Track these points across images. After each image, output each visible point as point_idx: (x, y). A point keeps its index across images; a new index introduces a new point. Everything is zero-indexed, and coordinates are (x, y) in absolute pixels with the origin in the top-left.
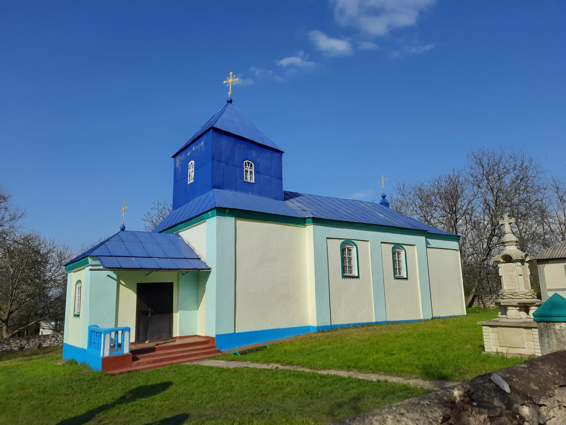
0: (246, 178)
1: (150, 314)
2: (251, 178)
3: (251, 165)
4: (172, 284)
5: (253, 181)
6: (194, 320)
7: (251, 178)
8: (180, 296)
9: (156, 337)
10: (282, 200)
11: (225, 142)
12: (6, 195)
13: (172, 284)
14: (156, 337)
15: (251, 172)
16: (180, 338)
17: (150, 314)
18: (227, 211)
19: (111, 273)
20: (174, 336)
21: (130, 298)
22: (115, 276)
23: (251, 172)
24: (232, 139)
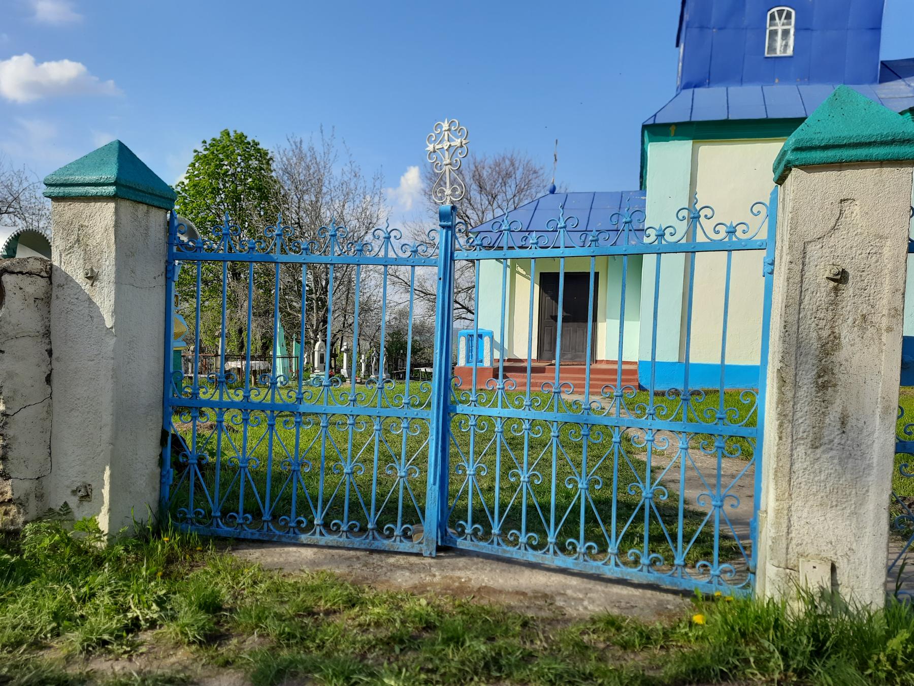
0: (772, 49)
2: (784, 46)
3: (788, 16)
5: (790, 52)
6: (620, 337)
7: (784, 46)
8: (608, 296)
9: (569, 356)
10: (873, 81)
12: (537, 168)
14: (569, 356)
15: (786, 33)
16: (608, 362)
18: (673, 129)
20: (599, 358)
21: (527, 292)
23: (786, 33)
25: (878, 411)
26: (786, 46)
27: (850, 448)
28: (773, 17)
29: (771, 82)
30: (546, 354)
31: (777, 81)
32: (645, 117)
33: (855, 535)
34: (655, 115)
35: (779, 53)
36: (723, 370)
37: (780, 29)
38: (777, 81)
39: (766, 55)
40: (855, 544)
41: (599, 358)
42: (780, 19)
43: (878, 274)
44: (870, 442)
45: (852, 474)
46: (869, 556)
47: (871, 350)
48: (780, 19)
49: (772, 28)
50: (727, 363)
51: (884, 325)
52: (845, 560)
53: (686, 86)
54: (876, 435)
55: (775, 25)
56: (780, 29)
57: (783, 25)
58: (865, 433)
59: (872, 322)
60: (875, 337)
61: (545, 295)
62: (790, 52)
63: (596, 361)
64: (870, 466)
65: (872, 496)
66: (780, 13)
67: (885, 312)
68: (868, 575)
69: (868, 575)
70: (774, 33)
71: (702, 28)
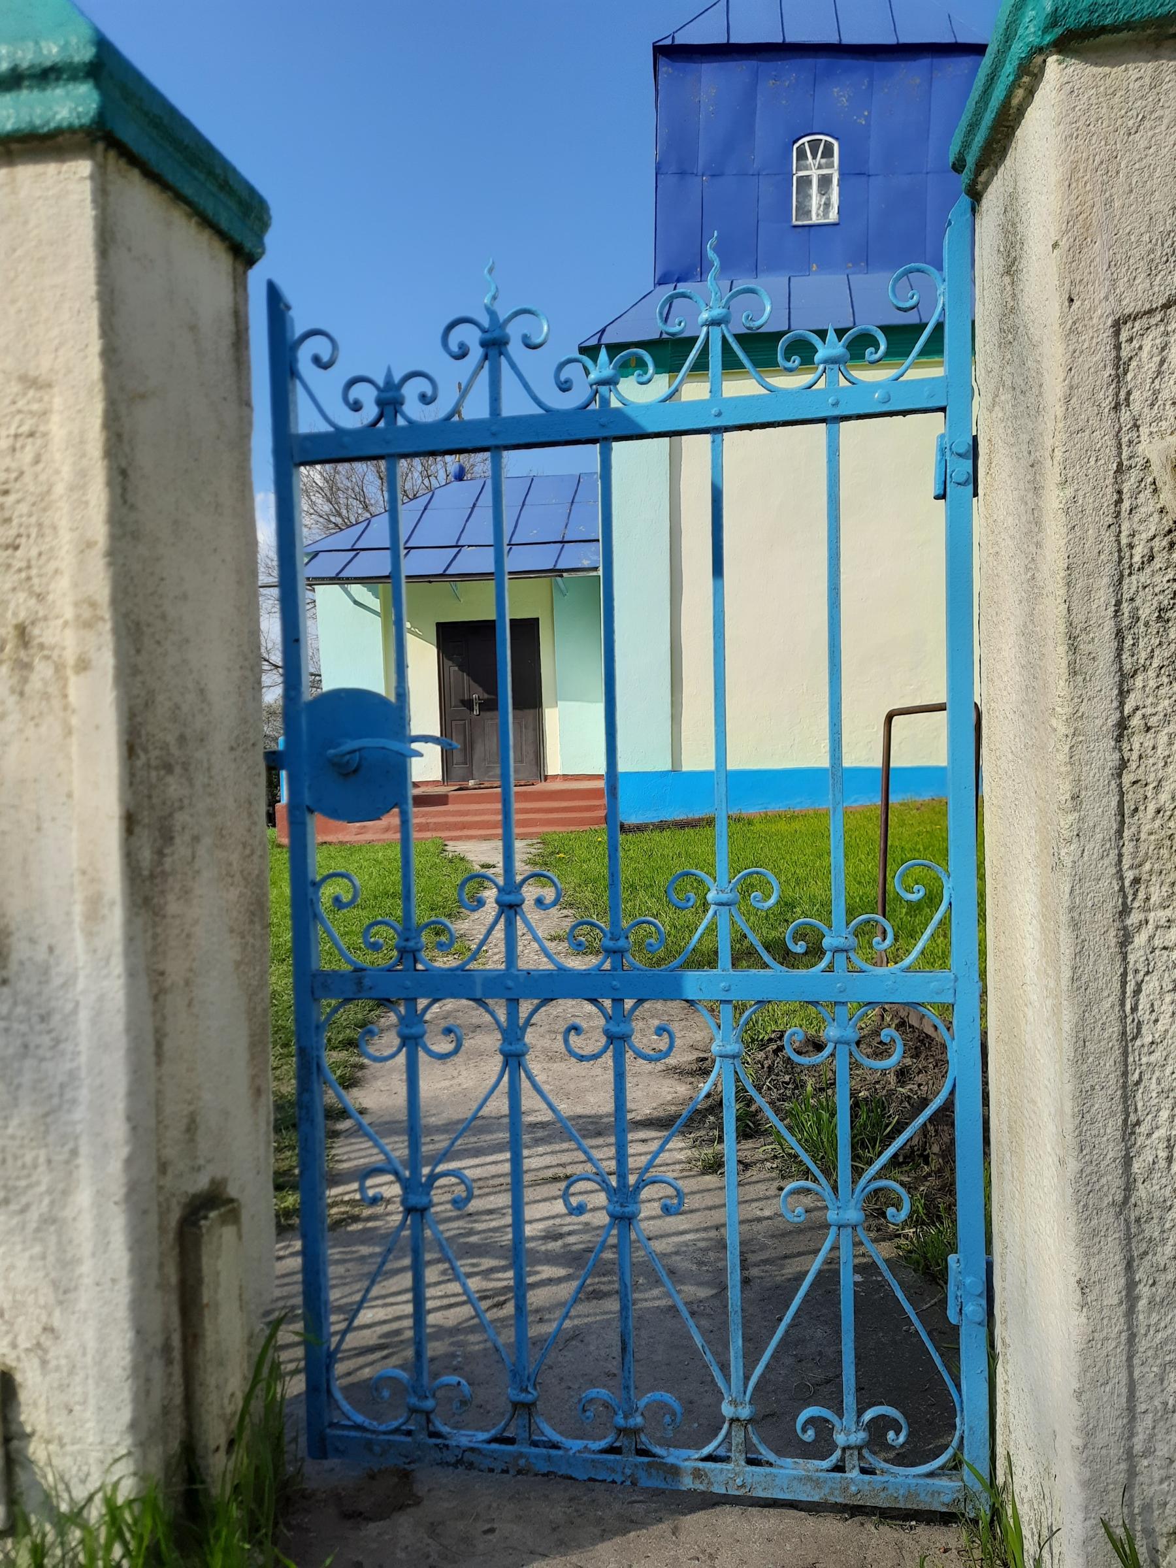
0: (804, 211)
1: (476, 708)
2: (824, 207)
3: (828, 152)
4: (536, 621)
5: (833, 216)
7: (824, 207)
11: (712, 84)
13: (536, 621)
15: (825, 181)
17: (476, 708)
19: (357, 590)
20: (551, 771)
22: (375, 604)
23: (825, 181)
24: (740, 69)
25: (78, 910)
26: (827, 205)
27: (24, 1028)
28: (801, 155)
29: (805, 270)
30: (458, 770)
31: (814, 268)
32: (661, 33)
33: (55, 1284)
34: (603, 331)
35: (815, 220)
36: (674, 778)
37: (815, 174)
38: (814, 268)
39: (795, 222)
40: (57, 1313)
41: (551, 771)
42: (814, 157)
43: (43, 501)
44: (69, 1006)
45: (34, 1103)
46: (92, 1345)
47: (43, 729)
48: (814, 157)
49: (801, 174)
50: (731, 766)
51: (70, 657)
52: (36, 1362)
53: (661, 281)
54: (81, 984)
55: (807, 168)
56: (815, 174)
57: (820, 167)
58: (57, 981)
59: (42, 646)
60: (53, 690)
61: (448, 663)
62: (833, 216)
63: (546, 778)
64: (72, 1075)
65: (85, 1167)
66: (814, 145)
67: (69, 613)
68: (92, 1402)
69: (92, 1402)
70: (805, 182)
71: (682, 173)
